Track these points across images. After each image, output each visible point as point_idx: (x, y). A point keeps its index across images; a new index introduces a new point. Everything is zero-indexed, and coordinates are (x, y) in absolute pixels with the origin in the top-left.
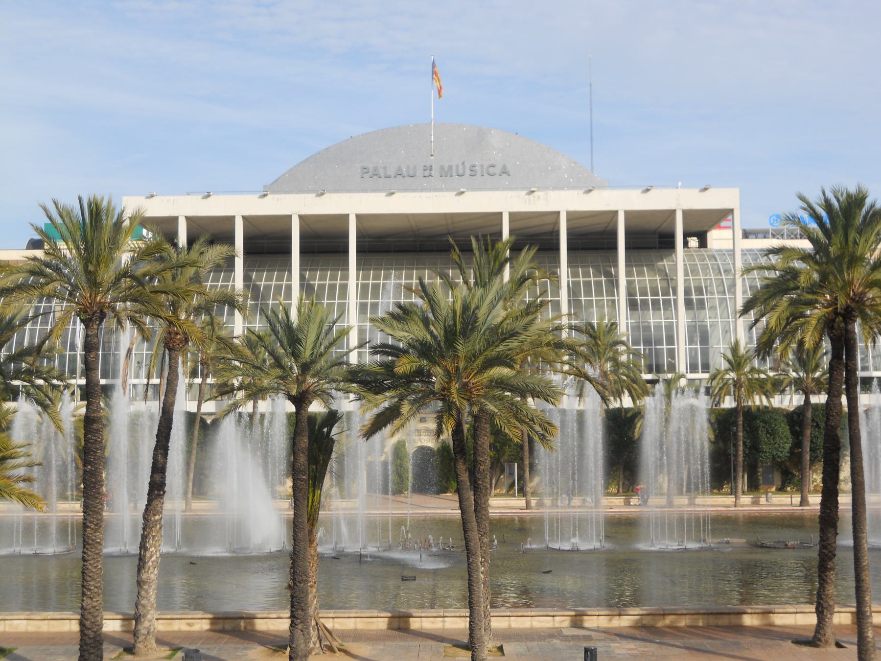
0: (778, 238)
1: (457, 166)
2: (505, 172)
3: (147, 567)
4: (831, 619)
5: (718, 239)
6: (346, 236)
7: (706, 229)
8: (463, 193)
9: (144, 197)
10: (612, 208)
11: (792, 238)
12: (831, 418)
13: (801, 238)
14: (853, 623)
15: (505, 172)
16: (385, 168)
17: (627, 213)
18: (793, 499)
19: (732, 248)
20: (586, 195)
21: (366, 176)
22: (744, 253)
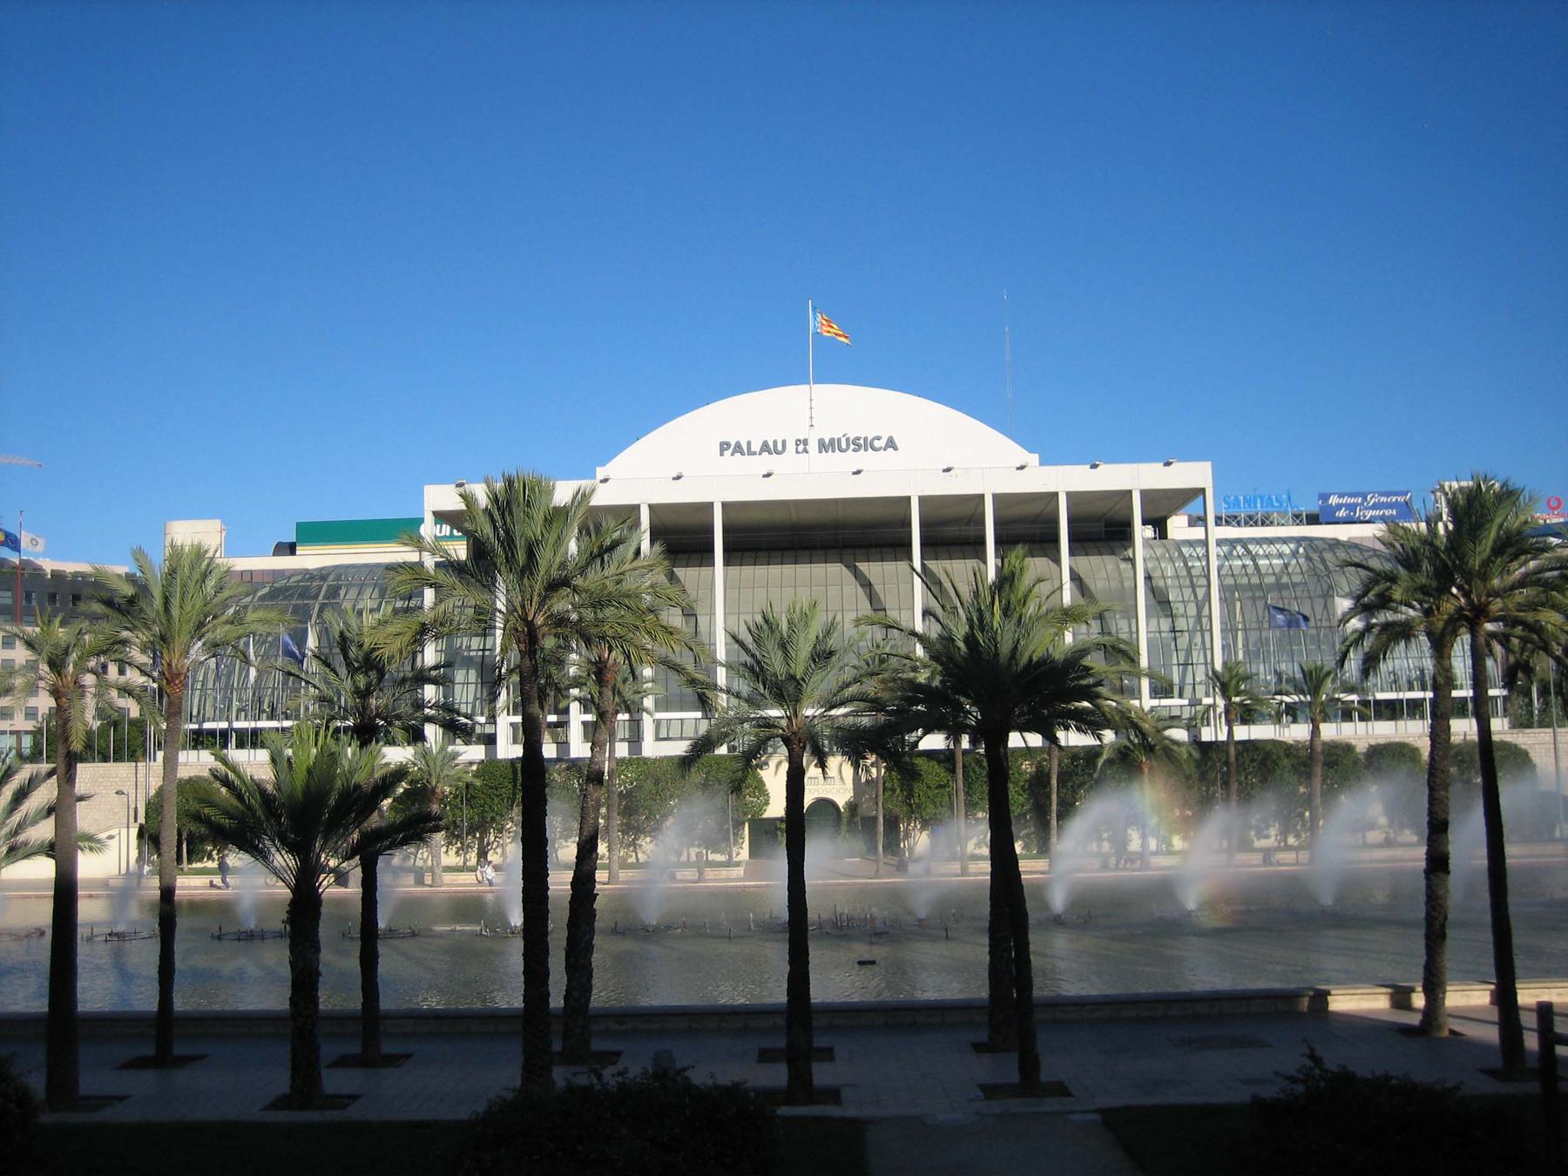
0: (1233, 526)
5: (1178, 527)
6: (1056, 522)
7: (1164, 514)
9: (1162, 464)
10: (1052, 489)
12: (1438, 745)
14: (1492, 1003)
15: (891, 444)
16: (749, 443)
17: (922, 500)
19: (1203, 537)
21: (728, 453)
22: (1220, 543)
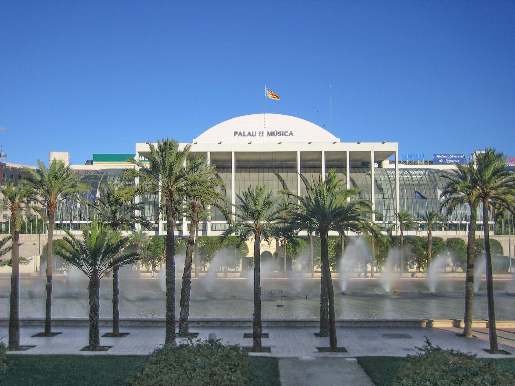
1: (274, 132)
2: (291, 134)
3: (484, 249)
4: (471, 325)
8: (360, 143)
9: (357, 143)
10: (344, 150)
11: (410, 164)
13: (414, 164)
16: (244, 132)
18: (250, 317)
19: (394, 168)
20: (383, 144)
21: (237, 135)
